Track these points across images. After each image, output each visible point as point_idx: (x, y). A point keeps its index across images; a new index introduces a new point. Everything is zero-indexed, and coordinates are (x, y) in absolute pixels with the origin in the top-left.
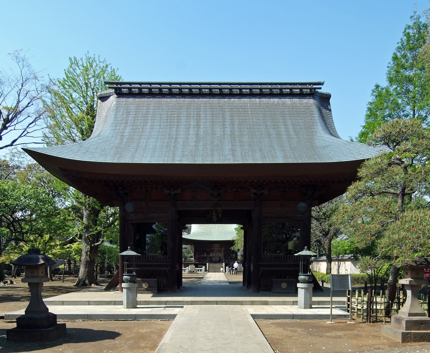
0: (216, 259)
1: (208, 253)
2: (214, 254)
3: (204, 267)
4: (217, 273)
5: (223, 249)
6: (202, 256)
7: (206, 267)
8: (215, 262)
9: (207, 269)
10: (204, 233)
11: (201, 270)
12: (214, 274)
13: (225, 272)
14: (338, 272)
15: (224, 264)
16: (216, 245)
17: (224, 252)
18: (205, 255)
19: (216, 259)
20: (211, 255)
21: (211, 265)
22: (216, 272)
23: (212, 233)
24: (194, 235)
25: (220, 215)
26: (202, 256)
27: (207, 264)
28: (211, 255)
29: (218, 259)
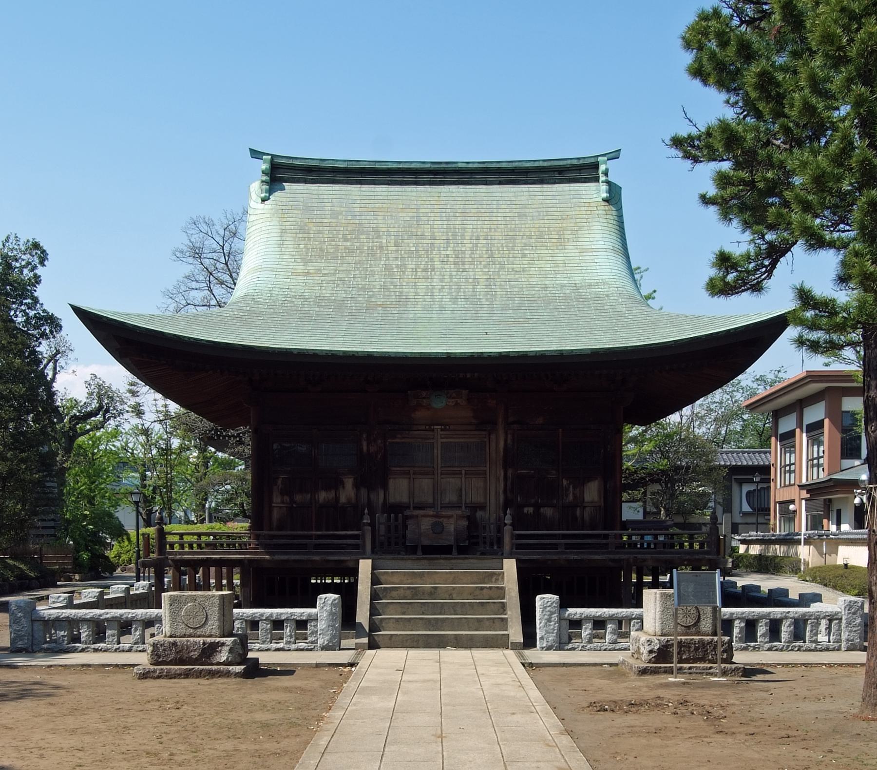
0: (437, 528)
1: (373, 475)
2: (425, 484)
3: (328, 601)
4: (451, 655)
5: (499, 442)
6: (323, 496)
7: (349, 596)
8: (435, 552)
9: (362, 616)
10: (339, 305)
11: (301, 624)
12: (422, 660)
13: (529, 640)
14: (862, 665)
15: (510, 566)
16: (439, 403)
17: (507, 464)
18: (348, 492)
19: (437, 528)
20: (399, 489)
21: (402, 576)
22: (440, 643)
23: (403, 301)
24: (251, 311)
25: (548, 512)
26: (323, 496)
27: (365, 566)
28: (399, 489)
29: (453, 525)
